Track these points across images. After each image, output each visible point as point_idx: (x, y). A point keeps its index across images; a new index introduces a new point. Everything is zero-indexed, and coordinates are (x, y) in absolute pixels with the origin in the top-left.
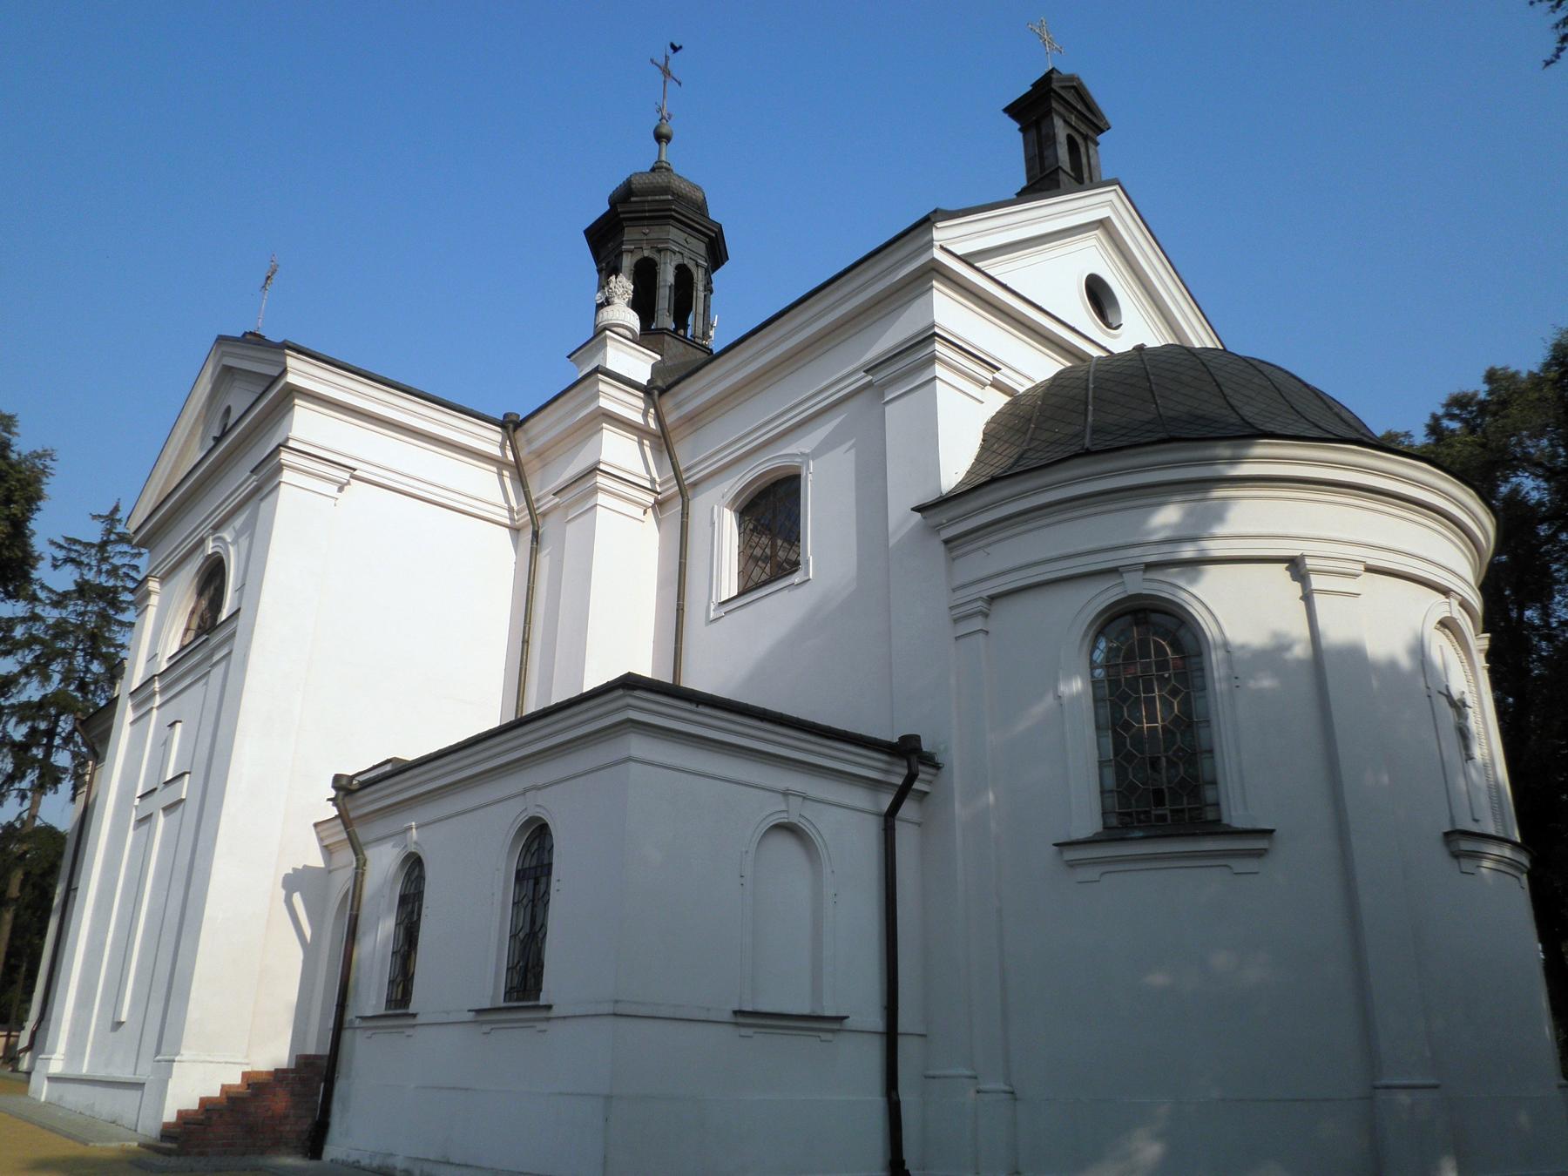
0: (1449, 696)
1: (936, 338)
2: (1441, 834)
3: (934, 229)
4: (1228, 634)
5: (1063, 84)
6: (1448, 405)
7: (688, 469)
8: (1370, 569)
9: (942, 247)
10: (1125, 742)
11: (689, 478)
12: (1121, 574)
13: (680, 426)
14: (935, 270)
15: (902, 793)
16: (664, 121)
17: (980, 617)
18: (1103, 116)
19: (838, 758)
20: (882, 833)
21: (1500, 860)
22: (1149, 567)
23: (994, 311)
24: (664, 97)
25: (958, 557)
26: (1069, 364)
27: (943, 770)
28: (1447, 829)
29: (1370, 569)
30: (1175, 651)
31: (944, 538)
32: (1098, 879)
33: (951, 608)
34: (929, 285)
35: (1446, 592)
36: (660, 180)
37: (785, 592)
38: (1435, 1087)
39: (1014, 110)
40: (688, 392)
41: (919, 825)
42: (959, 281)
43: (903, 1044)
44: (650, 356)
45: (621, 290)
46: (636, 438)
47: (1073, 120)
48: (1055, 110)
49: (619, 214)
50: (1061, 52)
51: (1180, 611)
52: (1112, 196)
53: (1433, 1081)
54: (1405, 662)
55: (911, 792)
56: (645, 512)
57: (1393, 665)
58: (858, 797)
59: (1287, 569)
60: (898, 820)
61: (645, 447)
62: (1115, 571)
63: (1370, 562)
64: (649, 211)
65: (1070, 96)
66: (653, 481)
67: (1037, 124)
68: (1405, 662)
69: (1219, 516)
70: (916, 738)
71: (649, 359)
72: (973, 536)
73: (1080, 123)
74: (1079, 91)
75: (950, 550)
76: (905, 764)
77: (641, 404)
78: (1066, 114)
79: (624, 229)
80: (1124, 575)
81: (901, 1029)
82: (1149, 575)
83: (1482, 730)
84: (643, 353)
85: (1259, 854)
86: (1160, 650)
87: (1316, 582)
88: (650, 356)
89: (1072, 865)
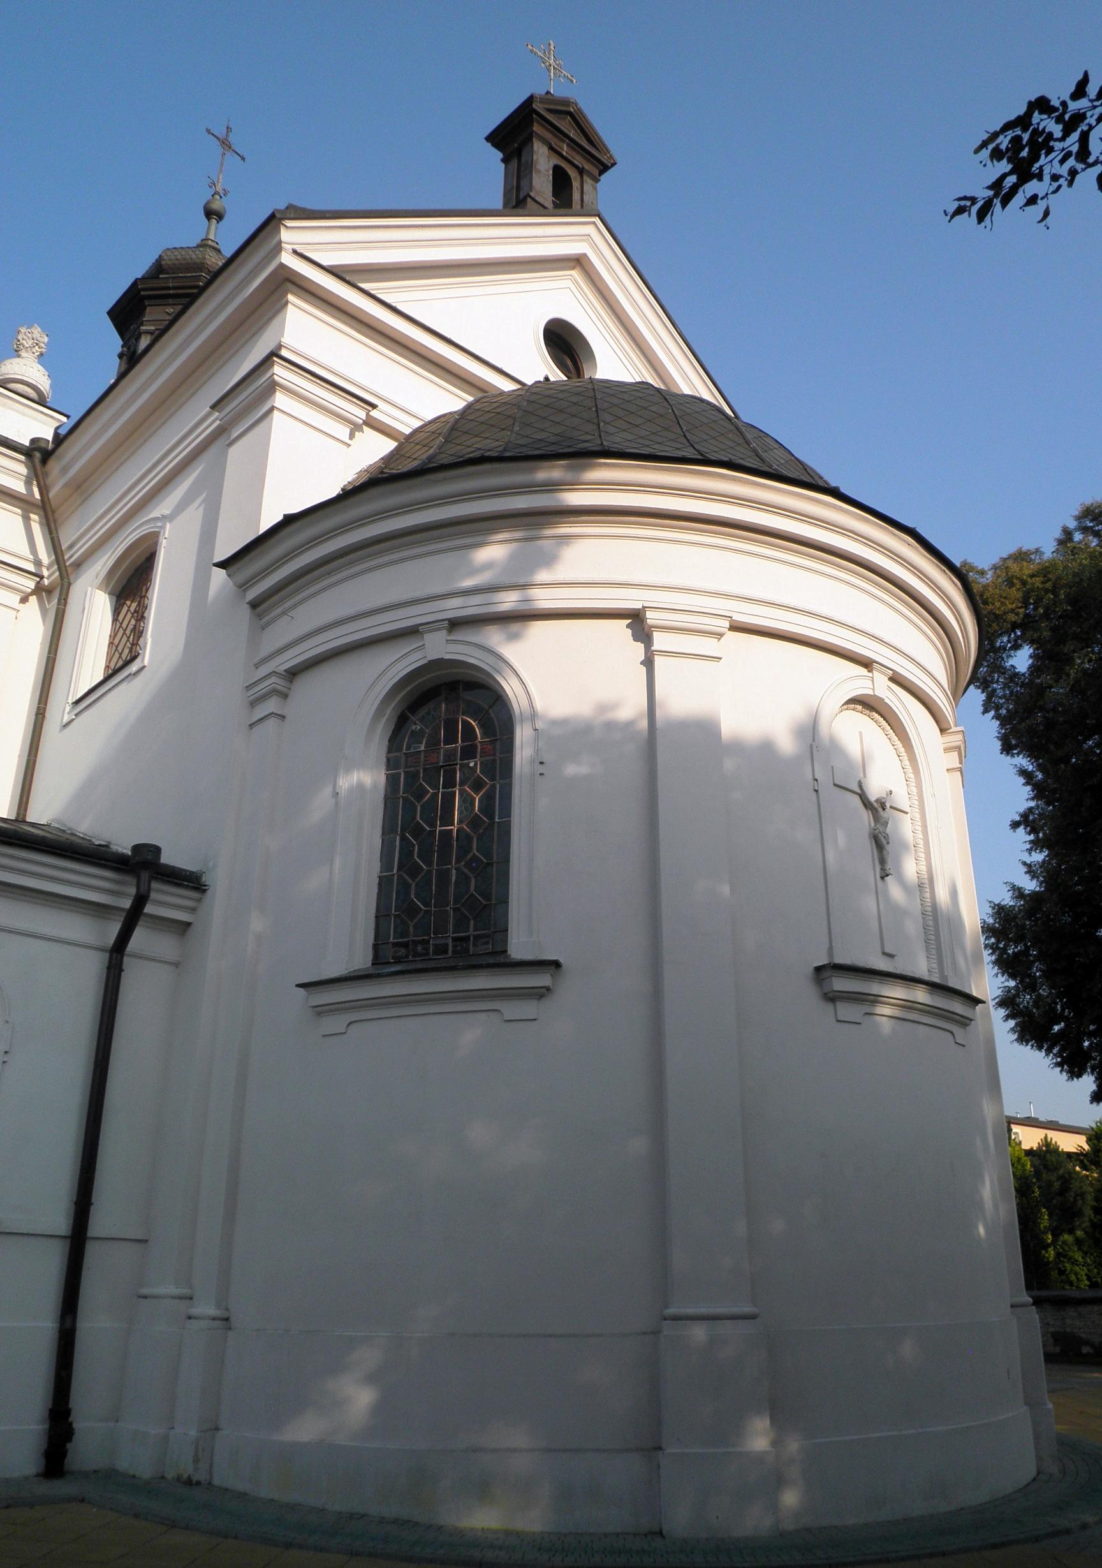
0: (863, 797)
1: (275, 359)
2: (810, 970)
3: (282, 229)
4: (539, 705)
5: (552, 107)
6: (1078, 518)
7: (71, 547)
8: (737, 628)
9: (295, 252)
10: (413, 851)
11: (71, 557)
12: (422, 634)
13: (70, 496)
14: (287, 281)
15: (133, 918)
16: (217, 197)
17: (275, 697)
18: (605, 146)
19: (25, 872)
20: (105, 971)
21: (909, 1005)
22: (455, 624)
23: (377, 336)
24: (221, 171)
25: (268, 624)
26: (471, 399)
27: (209, 893)
28: (824, 961)
29: (737, 628)
30: (485, 734)
31: (248, 601)
32: (344, 1031)
33: (248, 688)
34: (284, 301)
35: (867, 664)
36: (194, 256)
37: (124, 686)
38: (753, 1317)
39: (498, 138)
40: (70, 455)
41: (176, 965)
42: (313, 289)
43: (92, 1252)
44: (52, 417)
45: (30, 342)
46: (19, 511)
47: (565, 149)
48: (536, 133)
49: (140, 291)
50: (572, 81)
51: (490, 681)
52: (590, 230)
53: (748, 1309)
54: (786, 744)
55: (142, 918)
56: (24, 600)
57: (766, 748)
58: (76, 927)
59: (628, 626)
60: (129, 955)
61: (32, 523)
62: (413, 632)
63: (738, 617)
64: (174, 288)
65: (565, 125)
66: (38, 563)
67: (518, 153)
68: (786, 744)
69: (549, 560)
70: (157, 850)
71: (51, 420)
72: (275, 598)
73: (574, 154)
74: (577, 119)
75: (260, 616)
76: (134, 881)
77: (23, 470)
78: (554, 142)
79: (145, 309)
80: (424, 635)
81: (91, 1232)
82: (460, 635)
83: (921, 842)
84: (42, 413)
85: (541, 993)
86: (468, 730)
87: (660, 641)
88: (52, 417)
89: (320, 1011)
